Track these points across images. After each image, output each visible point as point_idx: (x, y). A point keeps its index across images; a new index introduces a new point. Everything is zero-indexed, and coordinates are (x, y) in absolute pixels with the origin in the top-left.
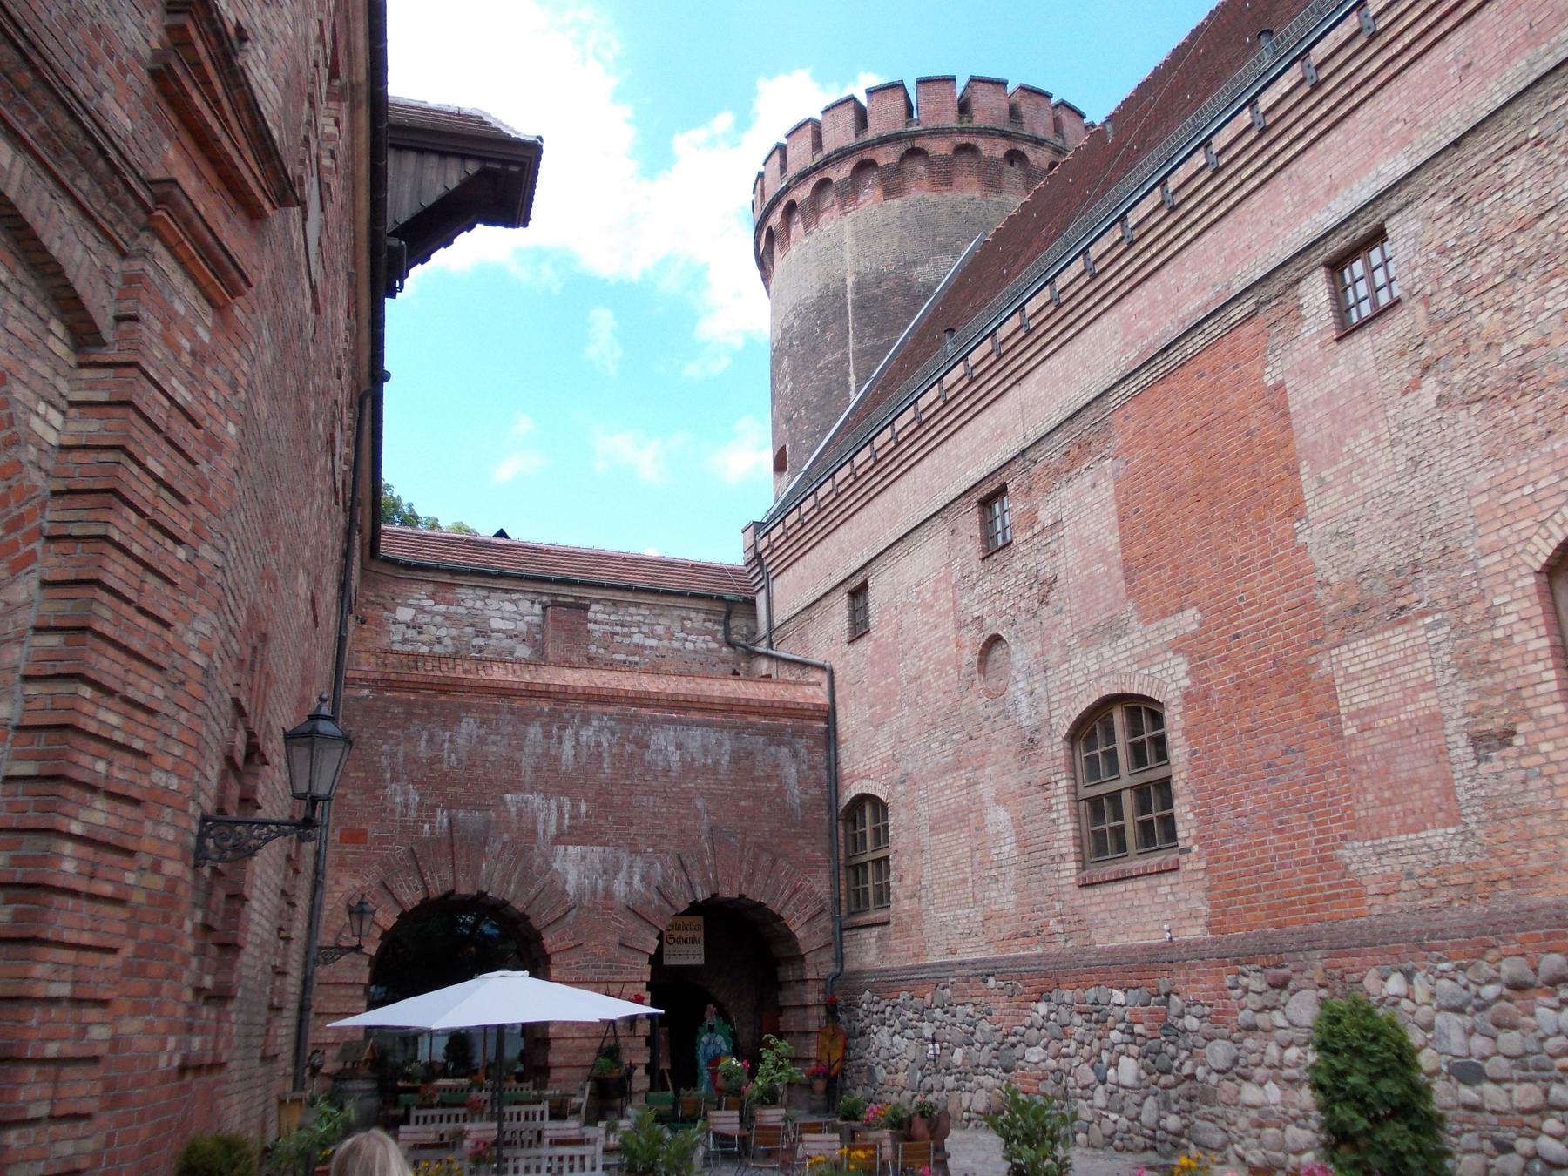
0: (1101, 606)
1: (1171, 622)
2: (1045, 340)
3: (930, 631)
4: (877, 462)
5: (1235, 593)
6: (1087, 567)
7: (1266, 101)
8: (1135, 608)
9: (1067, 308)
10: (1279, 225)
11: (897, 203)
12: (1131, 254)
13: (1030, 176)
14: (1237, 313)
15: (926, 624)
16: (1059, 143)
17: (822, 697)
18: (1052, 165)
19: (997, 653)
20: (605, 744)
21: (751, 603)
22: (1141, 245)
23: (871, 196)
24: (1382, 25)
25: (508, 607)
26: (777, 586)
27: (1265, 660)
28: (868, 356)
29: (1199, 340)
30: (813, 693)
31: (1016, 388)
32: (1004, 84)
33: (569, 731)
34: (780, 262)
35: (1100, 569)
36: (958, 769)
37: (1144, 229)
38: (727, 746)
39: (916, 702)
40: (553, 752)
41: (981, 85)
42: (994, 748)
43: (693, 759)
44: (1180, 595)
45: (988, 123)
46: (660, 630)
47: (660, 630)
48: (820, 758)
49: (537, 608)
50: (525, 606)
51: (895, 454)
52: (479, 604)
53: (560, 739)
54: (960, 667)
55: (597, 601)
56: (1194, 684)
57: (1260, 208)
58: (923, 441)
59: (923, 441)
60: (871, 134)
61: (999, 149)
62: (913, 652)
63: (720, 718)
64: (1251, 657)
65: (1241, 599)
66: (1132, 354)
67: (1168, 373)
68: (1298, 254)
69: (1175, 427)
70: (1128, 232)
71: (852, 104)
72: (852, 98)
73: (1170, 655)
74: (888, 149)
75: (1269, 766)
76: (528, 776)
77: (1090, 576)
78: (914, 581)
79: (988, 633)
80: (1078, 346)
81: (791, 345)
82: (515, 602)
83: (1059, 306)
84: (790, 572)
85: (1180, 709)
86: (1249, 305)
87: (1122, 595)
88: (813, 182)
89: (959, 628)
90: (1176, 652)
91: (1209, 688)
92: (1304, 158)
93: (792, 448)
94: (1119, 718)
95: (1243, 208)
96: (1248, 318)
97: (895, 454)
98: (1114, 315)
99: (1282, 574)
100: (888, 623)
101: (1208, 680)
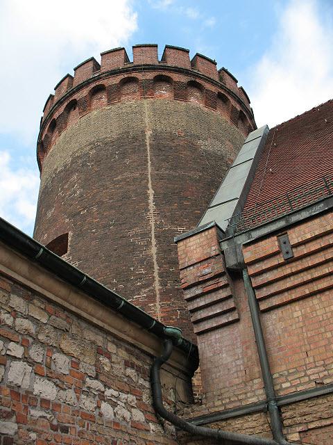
23: (164, 93)
46: (62, 363)
47: (62, 363)
88: (122, 77)
93: (76, 236)
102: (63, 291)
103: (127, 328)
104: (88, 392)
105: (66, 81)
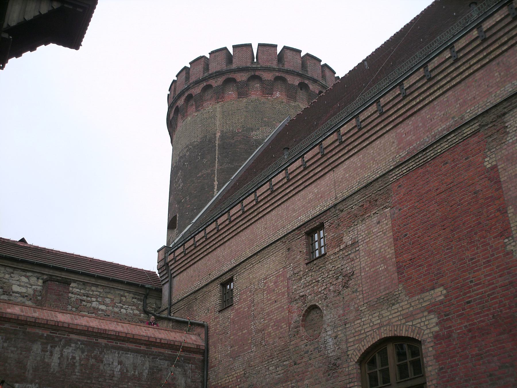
0: (382, 287)
1: (427, 296)
2: (351, 147)
3: (272, 303)
4: (244, 213)
5: (467, 279)
6: (373, 267)
7: (486, 25)
8: (404, 288)
9: (365, 130)
10: (492, 87)
11: (245, 100)
12: (404, 102)
13: (310, 95)
14: (467, 131)
15: (270, 300)
16: (324, 83)
17: (201, 343)
18: (320, 92)
19: (314, 315)
20: (78, 358)
21: (160, 291)
22: (411, 98)
23: (231, 93)
24: (461, 55)
25: (24, 279)
26: (176, 281)
27: (487, 315)
28: (225, 174)
29: (445, 145)
30: (193, 339)
31: (331, 172)
32: (300, 51)
33: (57, 349)
34: (181, 125)
35: (382, 267)
36: (286, 381)
37: (412, 89)
38: (147, 365)
39: (261, 343)
40: (46, 360)
41: (288, 51)
42: (310, 369)
43: (127, 371)
44: (431, 280)
45: (292, 69)
46: (108, 301)
47: (108, 301)
48: (198, 376)
49: (40, 282)
50: (33, 280)
51: (255, 208)
52: (7, 276)
53: (51, 354)
54: (290, 324)
55: (75, 281)
56: (441, 330)
57: (480, 79)
58: (273, 201)
59: (273, 201)
60: (234, 66)
61: (296, 81)
62: (261, 316)
63: (143, 348)
64: (478, 313)
65: (471, 282)
66: (403, 154)
67: (426, 162)
68: (505, 100)
69: (430, 190)
70: (359, 123)
71: (224, 51)
72: (225, 49)
73: (426, 313)
74: (242, 74)
75: (491, 375)
76: (29, 375)
77: (374, 272)
78: (263, 276)
79: (309, 305)
80: (370, 150)
81: (184, 165)
82: (27, 277)
83: (360, 129)
84: (185, 273)
85: (432, 344)
86: (476, 126)
87: (396, 281)
88: (202, 86)
89: (290, 302)
90: (429, 312)
91: (452, 331)
92: (507, 54)
94: (391, 350)
95: (470, 79)
96: (474, 133)
97: (255, 208)
98: (392, 134)
99: (498, 267)
100: (245, 300)
101: (450, 327)
102: (106, 283)
103: (132, 288)
104: (117, 307)
105: (184, 72)
